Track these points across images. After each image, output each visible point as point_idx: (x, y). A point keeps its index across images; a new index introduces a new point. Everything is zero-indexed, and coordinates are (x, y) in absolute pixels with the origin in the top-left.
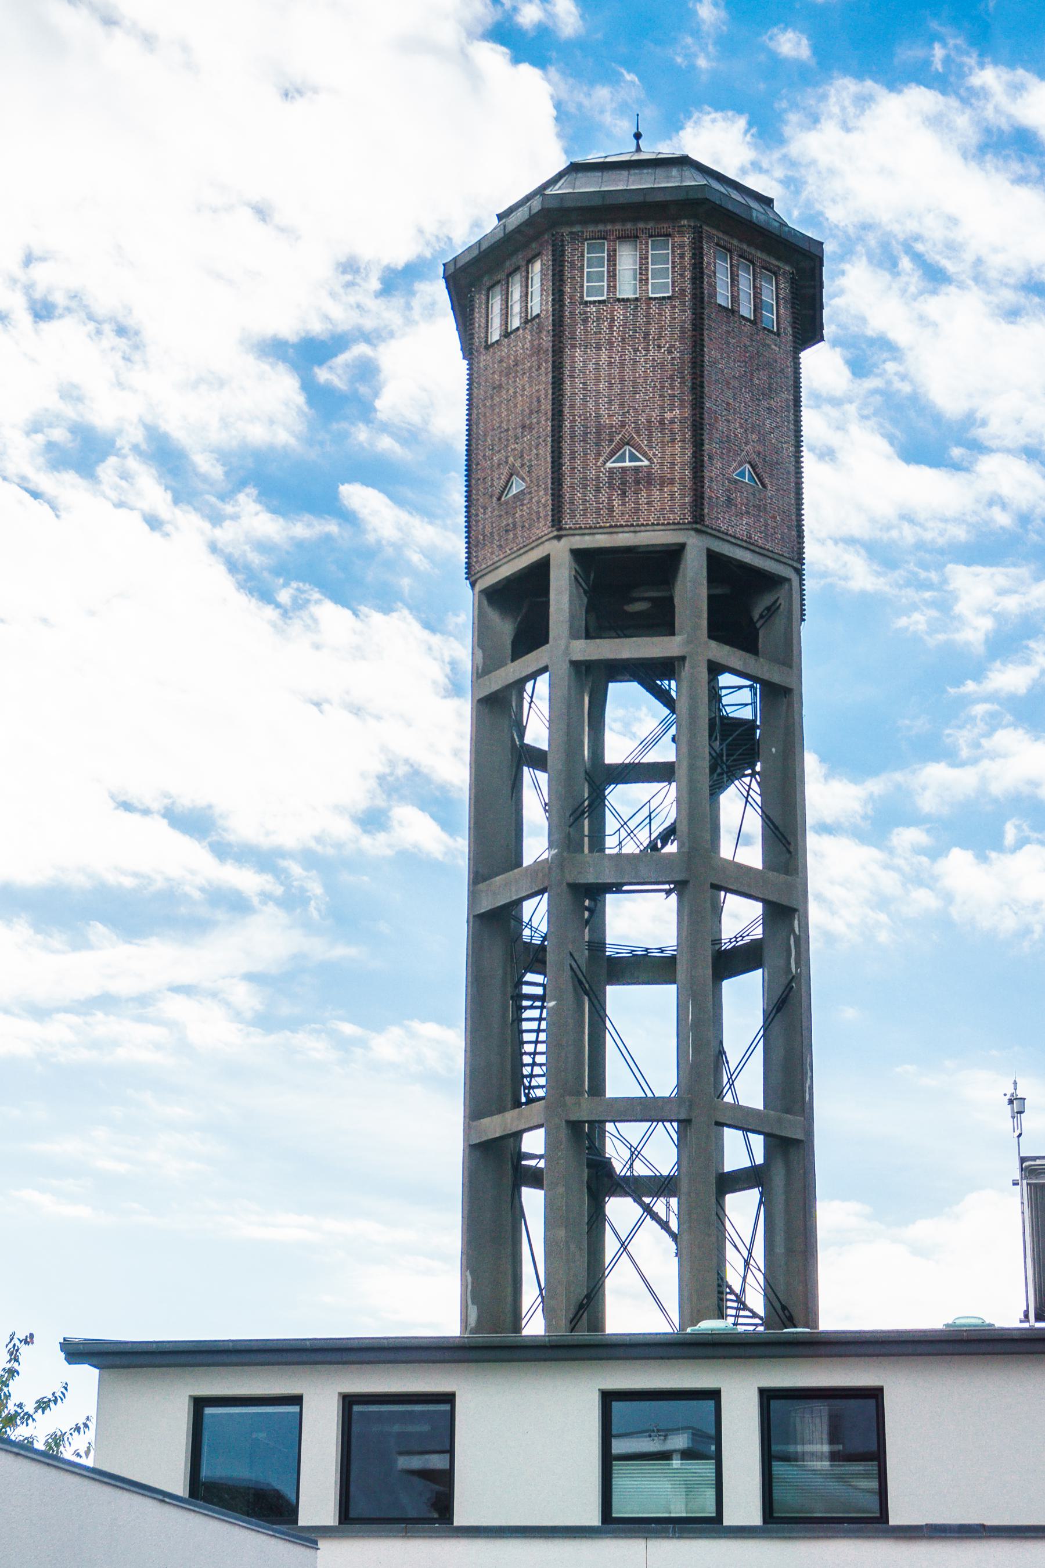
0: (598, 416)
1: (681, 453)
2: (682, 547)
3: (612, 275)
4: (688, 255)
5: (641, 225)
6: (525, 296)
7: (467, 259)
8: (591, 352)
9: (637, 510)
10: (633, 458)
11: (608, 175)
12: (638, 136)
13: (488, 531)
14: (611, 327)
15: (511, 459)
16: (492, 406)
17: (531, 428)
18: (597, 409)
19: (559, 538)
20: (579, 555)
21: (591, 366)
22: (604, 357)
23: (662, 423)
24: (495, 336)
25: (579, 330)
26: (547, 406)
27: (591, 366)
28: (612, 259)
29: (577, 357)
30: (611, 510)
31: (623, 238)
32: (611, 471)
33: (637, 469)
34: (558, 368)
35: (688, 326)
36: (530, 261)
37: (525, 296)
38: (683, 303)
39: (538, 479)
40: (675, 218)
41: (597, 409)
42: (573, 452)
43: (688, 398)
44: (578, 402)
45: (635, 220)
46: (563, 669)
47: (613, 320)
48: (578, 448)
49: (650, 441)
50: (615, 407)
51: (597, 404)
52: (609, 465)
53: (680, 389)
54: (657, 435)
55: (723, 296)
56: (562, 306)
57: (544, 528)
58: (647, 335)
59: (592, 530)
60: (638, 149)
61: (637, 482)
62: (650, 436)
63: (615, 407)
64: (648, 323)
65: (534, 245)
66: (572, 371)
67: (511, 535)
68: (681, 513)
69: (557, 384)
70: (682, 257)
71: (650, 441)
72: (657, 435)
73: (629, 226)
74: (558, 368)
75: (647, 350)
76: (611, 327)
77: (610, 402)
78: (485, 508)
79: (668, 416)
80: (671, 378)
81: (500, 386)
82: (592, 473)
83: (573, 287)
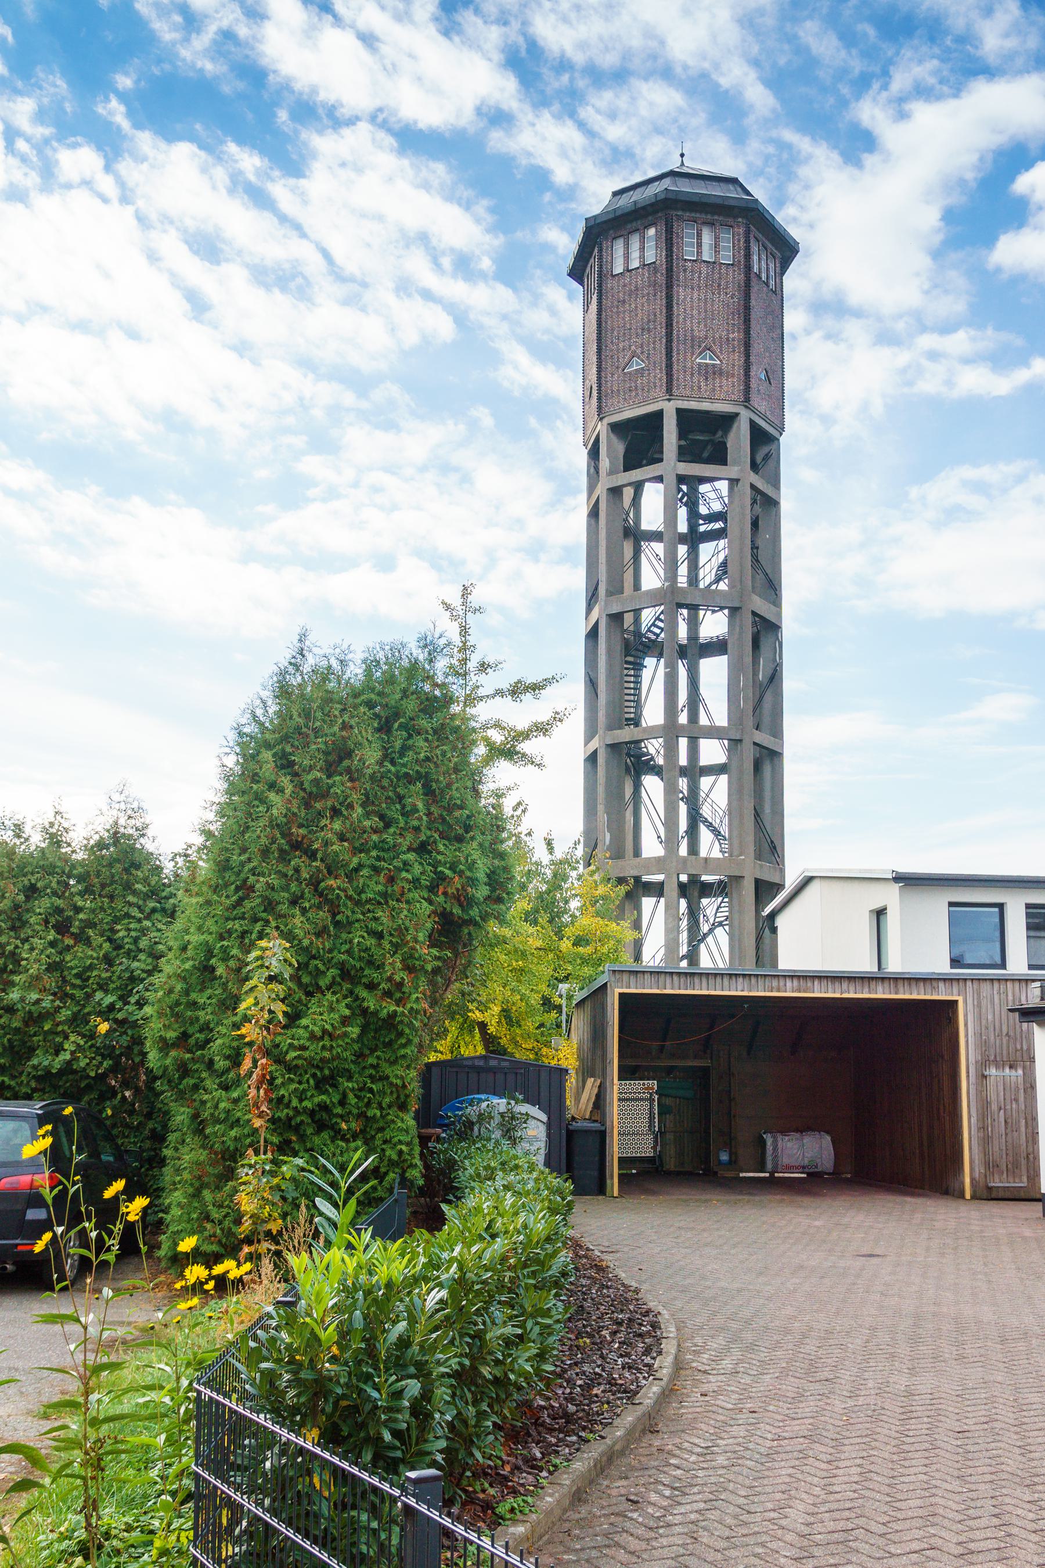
0: (692, 330)
1: (738, 359)
2: (737, 415)
3: (699, 245)
4: (742, 240)
5: (716, 217)
6: (642, 249)
7: (605, 219)
8: (689, 291)
9: (714, 390)
10: (711, 359)
11: (694, 182)
12: (682, 155)
13: (615, 388)
14: (699, 277)
15: (633, 348)
16: (618, 313)
17: (649, 330)
18: (692, 327)
19: (669, 400)
20: (680, 412)
21: (689, 299)
22: (695, 295)
23: (728, 339)
24: (618, 269)
25: (682, 275)
26: (662, 319)
27: (689, 299)
28: (699, 236)
29: (681, 293)
30: (700, 388)
31: (705, 223)
32: (699, 364)
33: (714, 365)
34: (669, 298)
35: (742, 283)
36: (647, 227)
37: (642, 249)
38: (739, 269)
39: (655, 363)
40: (735, 217)
41: (692, 327)
42: (678, 350)
43: (742, 327)
44: (681, 320)
45: (713, 214)
46: (671, 479)
47: (700, 273)
48: (681, 347)
49: (721, 350)
50: (702, 326)
51: (692, 323)
52: (698, 360)
53: (738, 321)
54: (725, 346)
55: (756, 269)
56: (672, 260)
57: (660, 391)
58: (719, 285)
59: (689, 398)
60: (682, 164)
61: (714, 374)
62: (721, 347)
63: (702, 326)
64: (720, 278)
65: (650, 218)
66: (678, 300)
67: (634, 393)
68: (738, 395)
69: (669, 307)
70: (739, 241)
71: (721, 350)
72: (725, 346)
73: (709, 217)
74: (669, 298)
75: (719, 293)
76: (699, 277)
77: (699, 323)
78: (613, 374)
79: (731, 336)
80: (733, 313)
81: (624, 302)
82: (689, 365)
83: (678, 249)
